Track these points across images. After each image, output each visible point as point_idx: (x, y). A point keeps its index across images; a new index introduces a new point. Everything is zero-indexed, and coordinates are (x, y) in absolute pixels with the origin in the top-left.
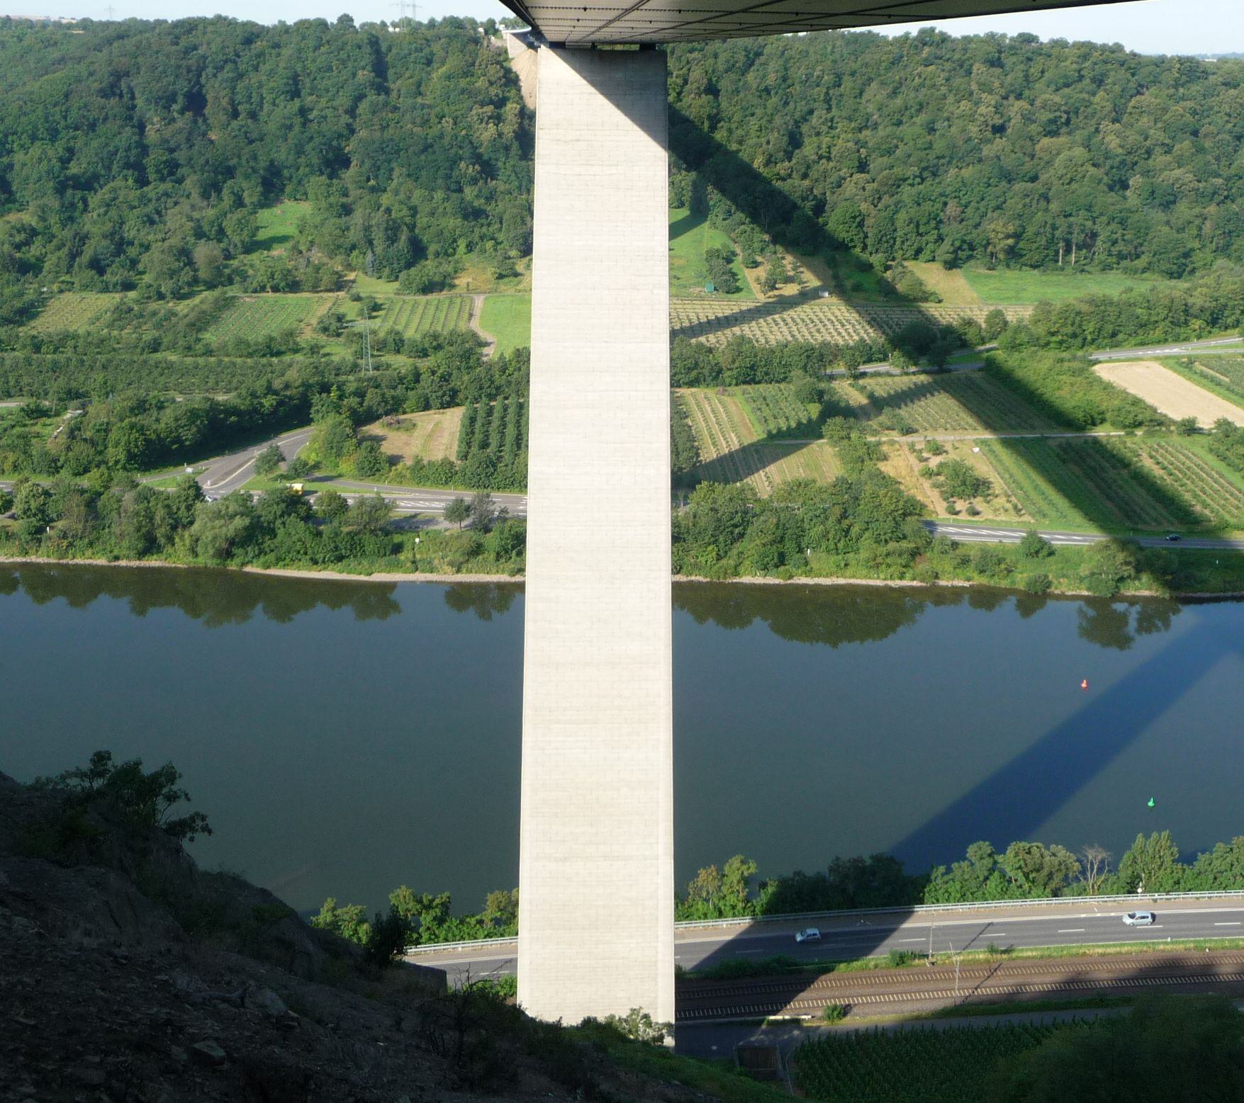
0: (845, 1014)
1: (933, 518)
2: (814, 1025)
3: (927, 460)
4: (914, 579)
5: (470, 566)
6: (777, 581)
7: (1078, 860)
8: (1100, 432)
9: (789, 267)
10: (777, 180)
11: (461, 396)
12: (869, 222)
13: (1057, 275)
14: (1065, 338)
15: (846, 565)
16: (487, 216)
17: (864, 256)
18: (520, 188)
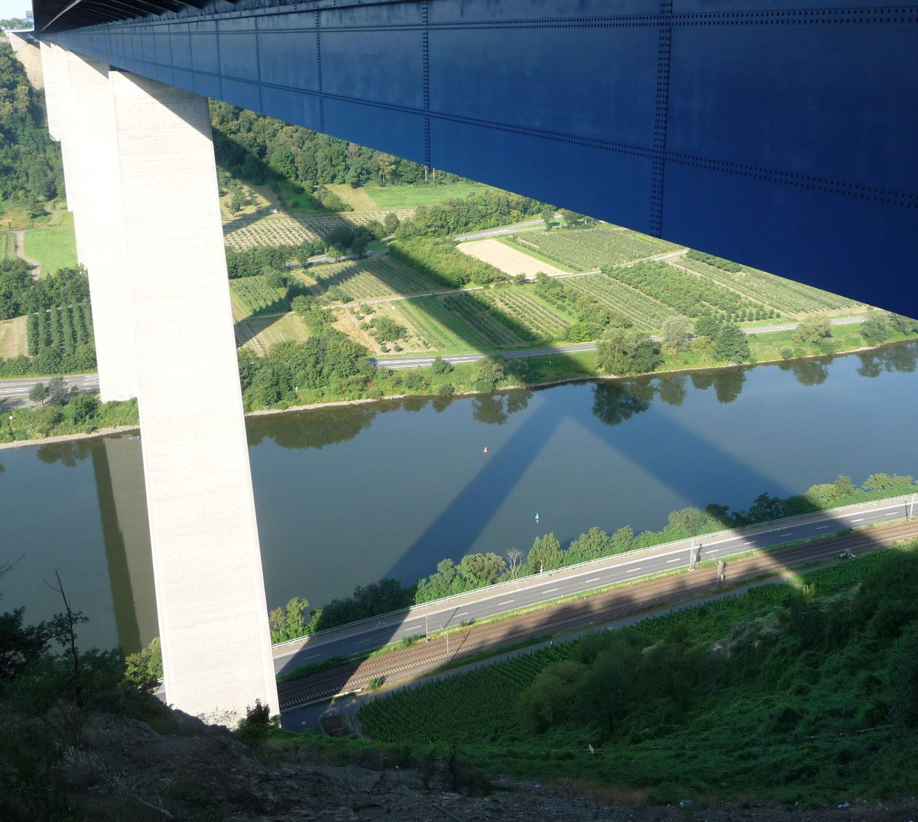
0: (382, 683)
1: (373, 356)
2: (364, 694)
3: (363, 318)
4: (368, 398)
5: (55, 431)
6: (278, 411)
7: (504, 560)
8: (469, 288)
9: (247, 194)
10: (230, 133)
11: (22, 308)
12: (298, 159)
13: (425, 187)
14: (437, 228)
15: (322, 394)
16: (15, 172)
17: (298, 183)
18: (37, 149)
